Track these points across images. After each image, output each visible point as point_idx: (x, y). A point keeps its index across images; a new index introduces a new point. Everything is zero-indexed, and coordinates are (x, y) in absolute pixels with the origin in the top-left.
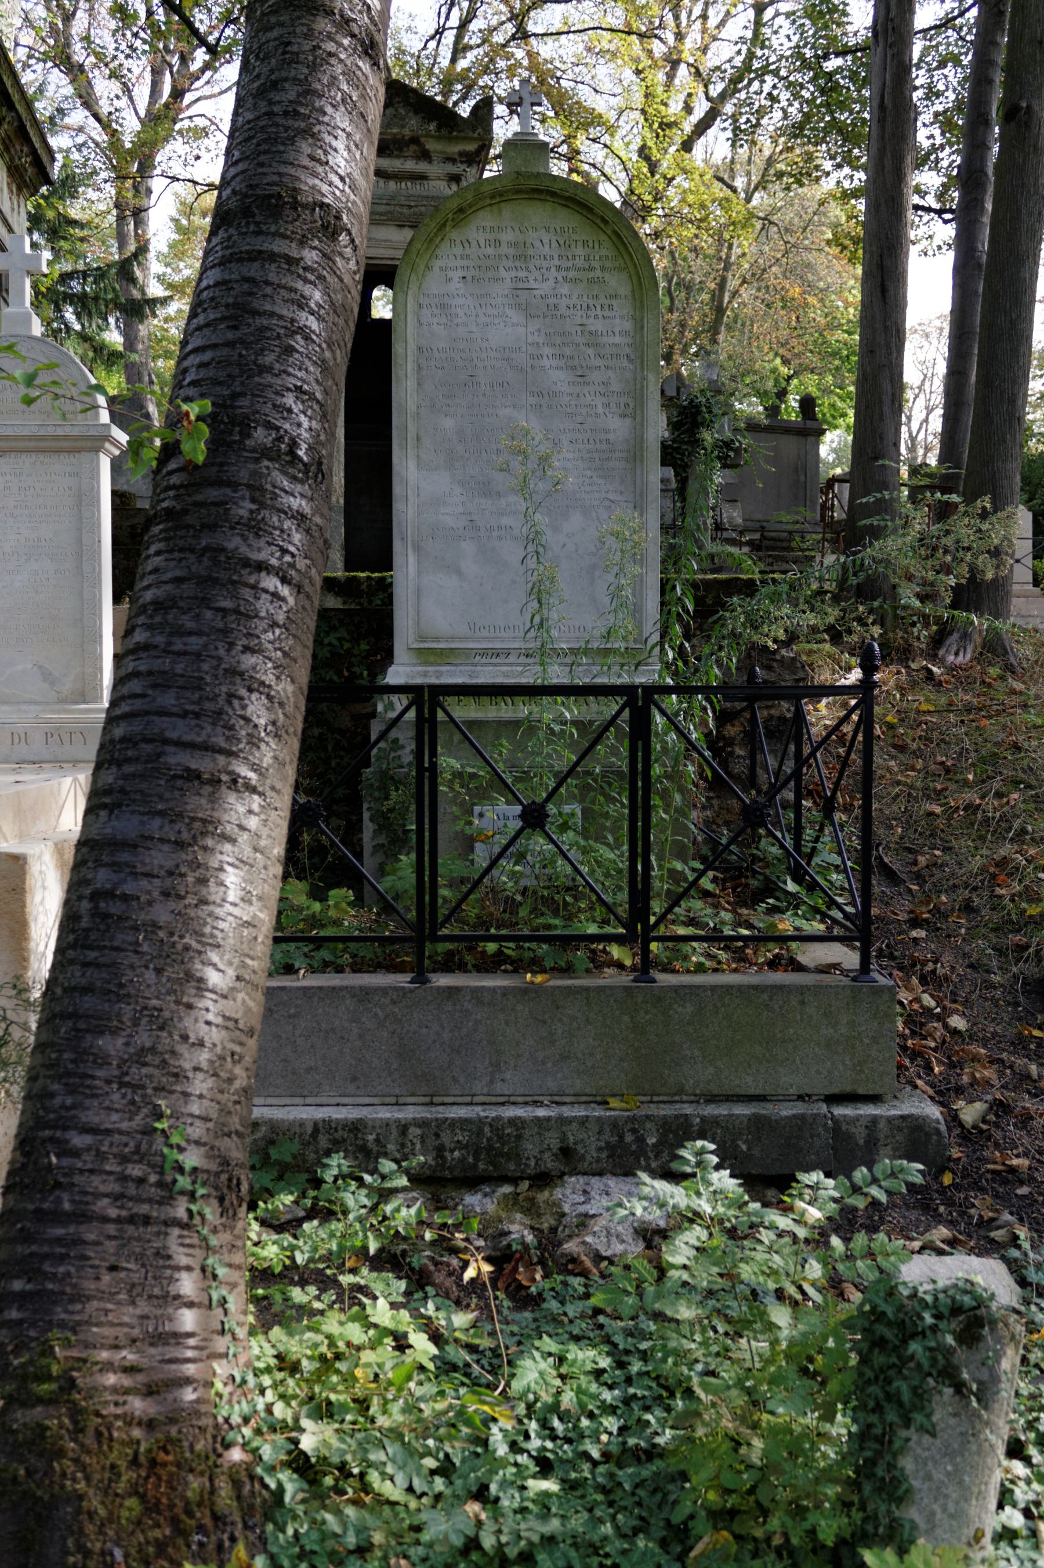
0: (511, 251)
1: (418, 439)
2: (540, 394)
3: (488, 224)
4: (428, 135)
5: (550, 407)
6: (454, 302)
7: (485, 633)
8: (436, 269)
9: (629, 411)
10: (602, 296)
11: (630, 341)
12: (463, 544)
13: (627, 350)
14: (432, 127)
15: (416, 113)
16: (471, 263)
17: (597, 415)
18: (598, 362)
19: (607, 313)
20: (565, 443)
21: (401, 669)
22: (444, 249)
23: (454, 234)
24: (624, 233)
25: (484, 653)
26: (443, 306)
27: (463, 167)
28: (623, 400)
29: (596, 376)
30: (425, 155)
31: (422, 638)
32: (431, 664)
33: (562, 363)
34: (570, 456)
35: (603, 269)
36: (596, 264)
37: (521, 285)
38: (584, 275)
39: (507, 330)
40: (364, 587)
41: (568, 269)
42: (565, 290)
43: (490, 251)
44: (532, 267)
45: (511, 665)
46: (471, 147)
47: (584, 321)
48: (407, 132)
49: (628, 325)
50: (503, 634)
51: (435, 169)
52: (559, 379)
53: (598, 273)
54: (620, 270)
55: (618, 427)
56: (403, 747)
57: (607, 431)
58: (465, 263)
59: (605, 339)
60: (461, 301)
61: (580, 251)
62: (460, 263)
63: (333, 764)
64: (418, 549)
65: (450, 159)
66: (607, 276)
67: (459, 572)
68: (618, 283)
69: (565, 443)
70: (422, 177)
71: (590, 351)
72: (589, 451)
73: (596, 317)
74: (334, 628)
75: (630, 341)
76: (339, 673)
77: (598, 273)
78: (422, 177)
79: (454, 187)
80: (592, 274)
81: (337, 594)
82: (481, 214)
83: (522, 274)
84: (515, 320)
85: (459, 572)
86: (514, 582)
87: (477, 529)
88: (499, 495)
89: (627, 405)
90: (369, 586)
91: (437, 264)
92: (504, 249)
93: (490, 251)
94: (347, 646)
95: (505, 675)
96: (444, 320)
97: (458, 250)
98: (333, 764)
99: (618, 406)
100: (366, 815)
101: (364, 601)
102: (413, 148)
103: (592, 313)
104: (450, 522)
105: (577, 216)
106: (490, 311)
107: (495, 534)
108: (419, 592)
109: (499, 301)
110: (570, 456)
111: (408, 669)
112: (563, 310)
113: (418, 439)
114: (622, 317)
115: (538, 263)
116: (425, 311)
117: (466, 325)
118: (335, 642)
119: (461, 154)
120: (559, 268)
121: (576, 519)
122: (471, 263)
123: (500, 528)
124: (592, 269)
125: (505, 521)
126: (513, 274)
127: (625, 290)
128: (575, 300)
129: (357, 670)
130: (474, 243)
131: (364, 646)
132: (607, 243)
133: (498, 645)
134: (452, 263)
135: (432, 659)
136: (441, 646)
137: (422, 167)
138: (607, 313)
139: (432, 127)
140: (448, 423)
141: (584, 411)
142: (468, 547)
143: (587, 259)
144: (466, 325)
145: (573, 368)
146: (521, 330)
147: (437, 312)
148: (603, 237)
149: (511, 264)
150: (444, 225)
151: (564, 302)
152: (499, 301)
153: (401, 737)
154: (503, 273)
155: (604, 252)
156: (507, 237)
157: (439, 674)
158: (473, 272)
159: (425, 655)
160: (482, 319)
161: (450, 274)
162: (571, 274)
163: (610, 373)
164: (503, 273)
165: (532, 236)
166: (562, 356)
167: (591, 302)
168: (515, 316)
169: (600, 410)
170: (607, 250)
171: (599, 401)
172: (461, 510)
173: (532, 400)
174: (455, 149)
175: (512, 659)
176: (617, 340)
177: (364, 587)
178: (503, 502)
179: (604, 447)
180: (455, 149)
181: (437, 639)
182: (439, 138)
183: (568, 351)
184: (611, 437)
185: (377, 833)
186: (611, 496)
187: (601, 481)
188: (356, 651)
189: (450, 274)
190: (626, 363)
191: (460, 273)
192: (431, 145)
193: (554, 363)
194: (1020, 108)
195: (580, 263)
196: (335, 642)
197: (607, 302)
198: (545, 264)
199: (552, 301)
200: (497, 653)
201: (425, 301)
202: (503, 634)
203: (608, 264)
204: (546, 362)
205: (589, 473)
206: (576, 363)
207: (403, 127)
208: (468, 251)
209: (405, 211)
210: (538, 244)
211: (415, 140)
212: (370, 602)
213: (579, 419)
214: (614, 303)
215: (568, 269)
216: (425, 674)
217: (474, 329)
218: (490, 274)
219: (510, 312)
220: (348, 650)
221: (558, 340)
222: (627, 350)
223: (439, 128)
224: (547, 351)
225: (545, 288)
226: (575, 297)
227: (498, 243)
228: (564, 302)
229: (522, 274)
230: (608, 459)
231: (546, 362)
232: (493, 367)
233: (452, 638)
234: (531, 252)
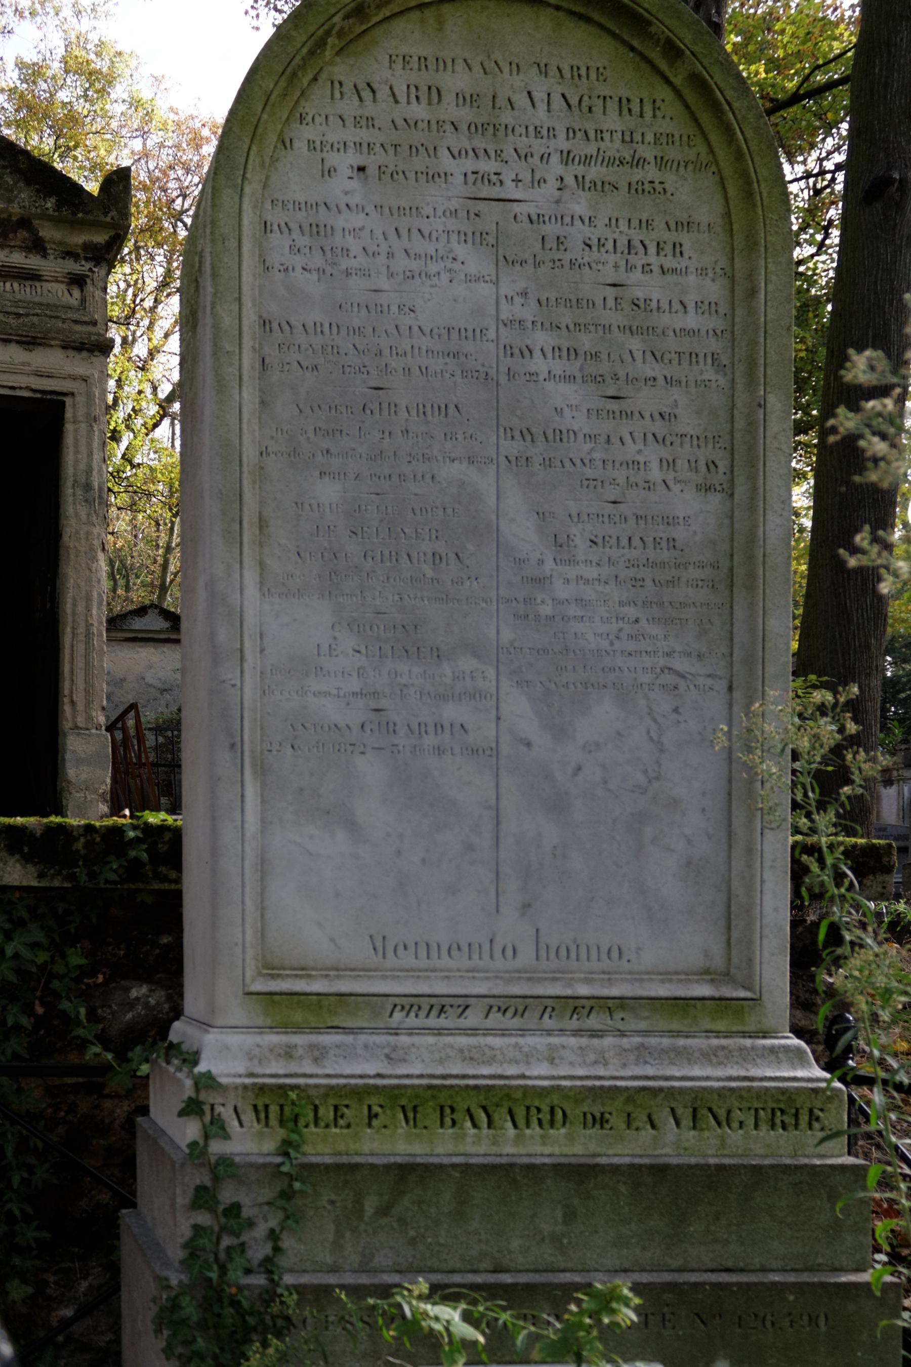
0: (465, 114)
1: (262, 524)
2: (527, 434)
3: (416, 51)
4: (44, 216)
5: (548, 463)
6: (341, 221)
7: (407, 959)
8: (301, 145)
9: (719, 477)
10: (659, 223)
11: (718, 323)
12: (361, 762)
13: (713, 345)
14: (50, 204)
15: (28, 183)
16: (376, 137)
17: (649, 486)
18: (651, 369)
19: (669, 262)
20: (581, 543)
22: (318, 101)
23: (340, 70)
24: (717, 78)
25: (411, 1004)
26: (316, 229)
27: (88, 265)
28: (703, 455)
29: (645, 400)
30: (38, 246)
31: (271, 969)
32: (298, 1029)
33: (574, 367)
34: (591, 572)
35: (661, 162)
36: (647, 152)
37: (486, 191)
38: (622, 176)
39: (457, 290)
40: (80, 845)
41: (587, 160)
42: (579, 205)
43: (418, 111)
44: (509, 153)
45: (473, 1031)
46: (100, 238)
47: (622, 276)
48: (15, 208)
49: (715, 290)
51: (51, 265)
52: (568, 401)
53: (651, 173)
54: (699, 167)
55: (695, 513)
56: (251, 1224)
57: (669, 521)
58: (364, 135)
59: (665, 320)
60: (358, 220)
61: (612, 121)
62: (352, 134)
64: (262, 770)
65: (69, 254)
66: (671, 179)
67: (352, 826)
68: (694, 197)
69: (581, 543)
70: (33, 276)
71: (635, 344)
72: (632, 564)
73: (646, 269)
74: (20, 923)
75: (718, 323)
77: (651, 173)
78: (33, 276)
79: (76, 293)
80: (638, 174)
81: (27, 859)
82: (399, 25)
83: (488, 166)
84: (472, 267)
85: (352, 826)
86: (470, 848)
87: (391, 728)
88: (438, 655)
89: (712, 465)
90: (89, 845)
91: (304, 134)
92: (450, 110)
93: (418, 111)
94: (42, 957)
95: (466, 1056)
96: (318, 261)
97: (349, 106)
99: (693, 465)
101: (82, 874)
102: (22, 234)
103: (638, 260)
104: (332, 711)
105: (608, 43)
106: (419, 245)
107: (429, 740)
108: (263, 865)
109: (438, 224)
110: (591, 572)
111: (250, 1040)
112: (576, 251)
113: (262, 524)
114: (702, 272)
115: (522, 143)
116: (276, 238)
117: (365, 273)
119: (87, 247)
120: (567, 158)
121: (604, 713)
122: (376, 137)
123: (439, 727)
124: (638, 162)
125: (451, 712)
126: (469, 164)
127: (707, 212)
128: (601, 230)
130: (383, 93)
131: (76, 959)
132: (671, 106)
133: (440, 988)
134: (335, 135)
135: (298, 1017)
136: (317, 986)
137: (34, 262)
138: (669, 262)
139: (50, 204)
140: (328, 492)
141: (621, 475)
142: (371, 770)
143: (628, 139)
144: (365, 273)
145: (598, 380)
146: (486, 290)
147: (302, 241)
148: (664, 93)
149: (461, 141)
150: (321, 44)
151: (578, 233)
152: (438, 224)
153: (245, 1200)
154: (447, 162)
155: (664, 127)
156: (456, 81)
157: (319, 1054)
158: (388, 159)
159: (286, 1010)
160: (402, 263)
161: (333, 159)
162: (594, 172)
163: (676, 394)
164: (447, 162)
165: (511, 84)
166: (573, 352)
167: (637, 236)
168: (474, 261)
169: (655, 474)
170: (671, 121)
171: (653, 454)
172: (354, 684)
173: (512, 448)
174: (79, 239)
175: (472, 1019)
176: (691, 321)
177: (80, 845)
178: (447, 669)
179: (666, 555)
180: (79, 239)
181: (303, 971)
182: (57, 222)
183: (586, 342)
184: (680, 533)
186: (679, 664)
187: (655, 630)
188: (59, 968)
189: (333, 159)
190: (710, 374)
191: (352, 158)
192: (47, 232)
193: (559, 366)
194: (889, 181)
195: (613, 147)
197: (671, 237)
198: (538, 146)
199: (551, 229)
200: (440, 1005)
201: (275, 217)
202: (446, 961)
203: (673, 153)
204: (539, 364)
205: (631, 612)
206: (604, 367)
207: (10, 201)
208: (370, 109)
209: (11, 320)
210: (522, 101)
211: (25, 223)
212: (92, 875)
213: (612, 493)
214: (685, 238)
215: (587, 160)
217: (383, 283)
218: (420, 162)
219: (461, 251)
221: (566, 317)
222: (713, 345)
223: (58, 207)
224: (542, 339)
225: (539, 199)
226: (602, 221)
227: (436, 93)
228: (578, 233)
229: (488, 166)
230: (673, 582)
231: (539, 364)
232: (424, 371)
233: (337, 970)
234: (507, 117)
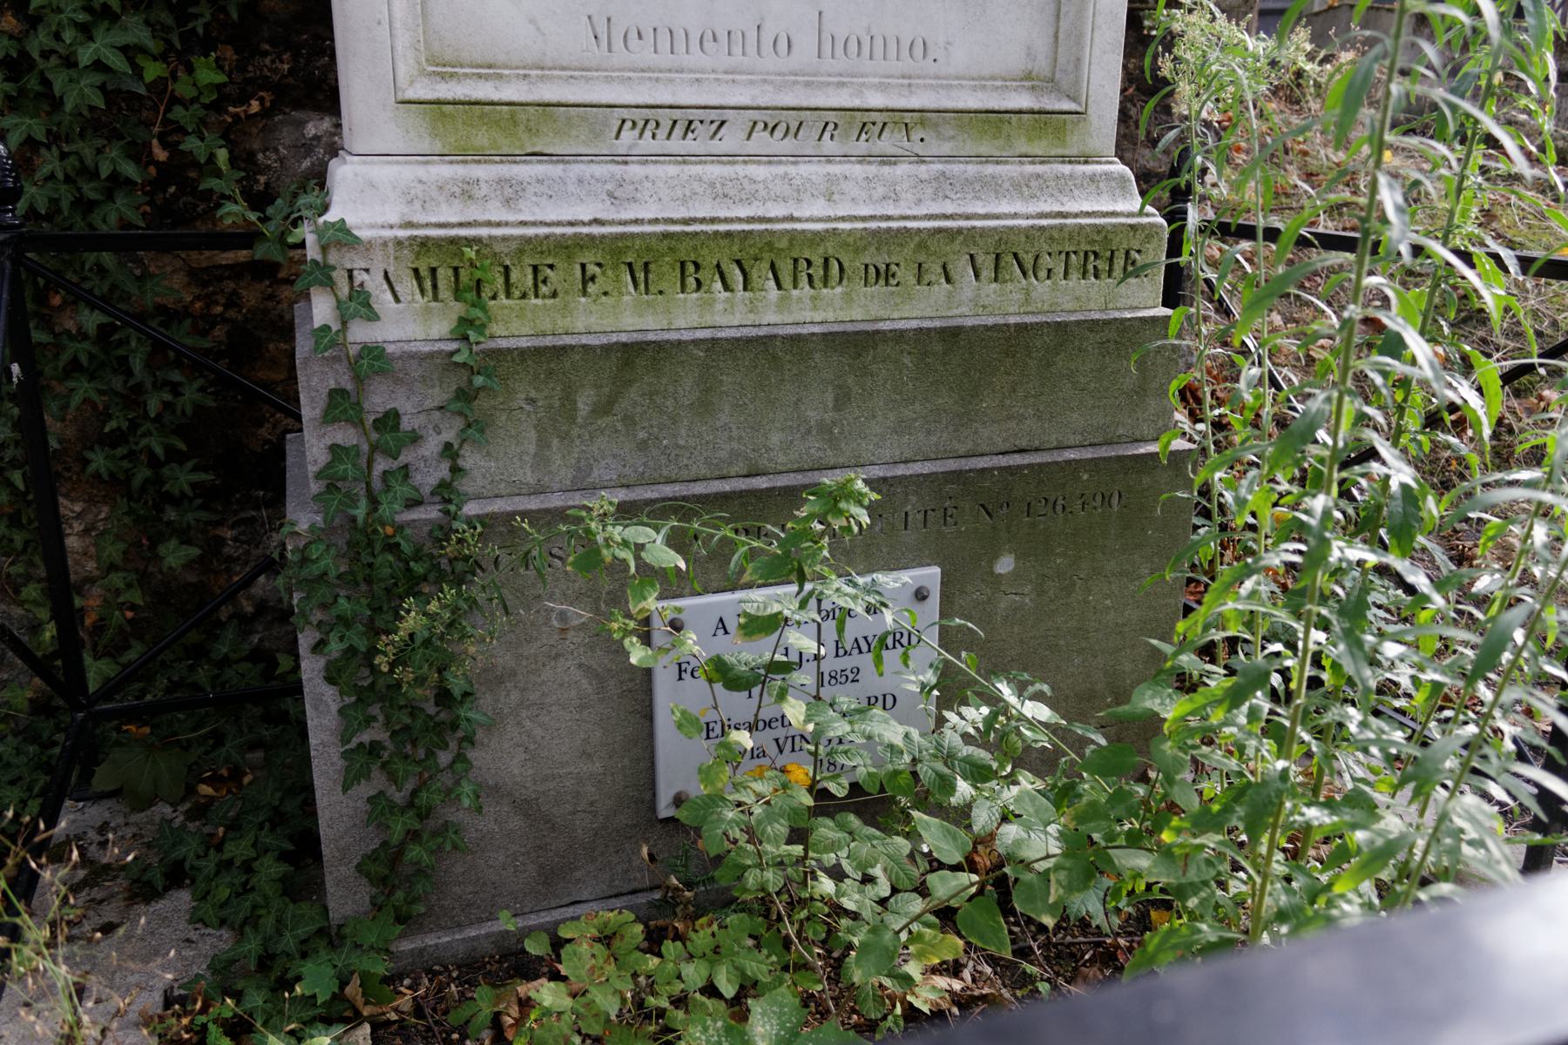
7: (642, 53)
21: (383, 172)
25: (646, 118)
31: (442, 66)
32: (482, 156)
45: (731, 158)
50: (696, 58)
56: (415, 438)
63: (153, 406)
76: (139, 153)
94: (153, 70)
98: (153, 406)
100: (311, 668)
111: (409, 172)
118: (117, 62)
129: (191, 144)
131: (208, 74)
133: (687, 95)
135: (481, 139)
136: (511, 92)
157: (512, 193)
175: (731, 140)
181: (489, 69)
185: (350, 719)
188: (183, 89)
196: (117, 62)
202: (696, 58)
216: (467, 192)
220: (159, 86)
233: (542, 68)
